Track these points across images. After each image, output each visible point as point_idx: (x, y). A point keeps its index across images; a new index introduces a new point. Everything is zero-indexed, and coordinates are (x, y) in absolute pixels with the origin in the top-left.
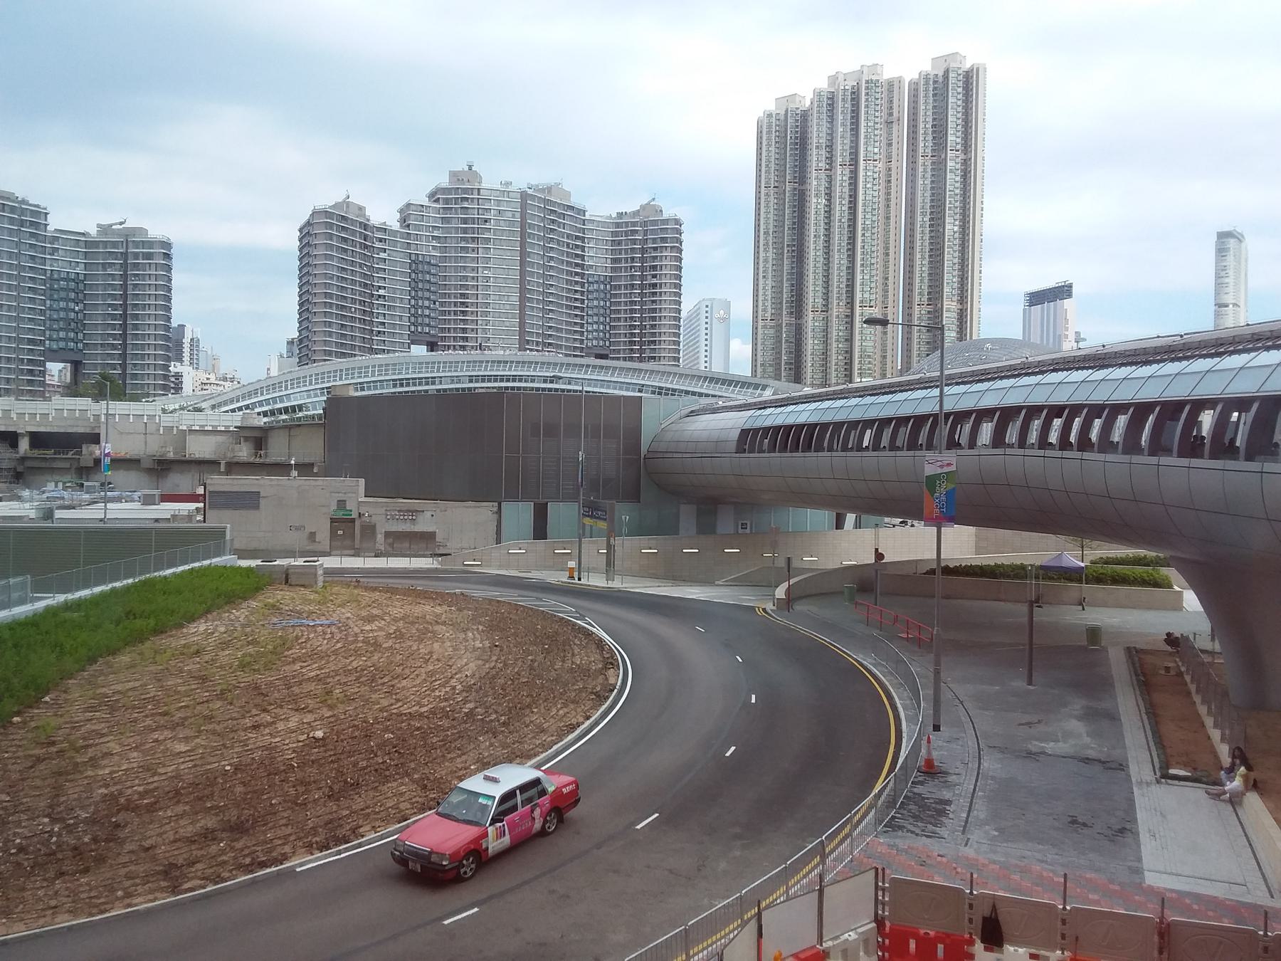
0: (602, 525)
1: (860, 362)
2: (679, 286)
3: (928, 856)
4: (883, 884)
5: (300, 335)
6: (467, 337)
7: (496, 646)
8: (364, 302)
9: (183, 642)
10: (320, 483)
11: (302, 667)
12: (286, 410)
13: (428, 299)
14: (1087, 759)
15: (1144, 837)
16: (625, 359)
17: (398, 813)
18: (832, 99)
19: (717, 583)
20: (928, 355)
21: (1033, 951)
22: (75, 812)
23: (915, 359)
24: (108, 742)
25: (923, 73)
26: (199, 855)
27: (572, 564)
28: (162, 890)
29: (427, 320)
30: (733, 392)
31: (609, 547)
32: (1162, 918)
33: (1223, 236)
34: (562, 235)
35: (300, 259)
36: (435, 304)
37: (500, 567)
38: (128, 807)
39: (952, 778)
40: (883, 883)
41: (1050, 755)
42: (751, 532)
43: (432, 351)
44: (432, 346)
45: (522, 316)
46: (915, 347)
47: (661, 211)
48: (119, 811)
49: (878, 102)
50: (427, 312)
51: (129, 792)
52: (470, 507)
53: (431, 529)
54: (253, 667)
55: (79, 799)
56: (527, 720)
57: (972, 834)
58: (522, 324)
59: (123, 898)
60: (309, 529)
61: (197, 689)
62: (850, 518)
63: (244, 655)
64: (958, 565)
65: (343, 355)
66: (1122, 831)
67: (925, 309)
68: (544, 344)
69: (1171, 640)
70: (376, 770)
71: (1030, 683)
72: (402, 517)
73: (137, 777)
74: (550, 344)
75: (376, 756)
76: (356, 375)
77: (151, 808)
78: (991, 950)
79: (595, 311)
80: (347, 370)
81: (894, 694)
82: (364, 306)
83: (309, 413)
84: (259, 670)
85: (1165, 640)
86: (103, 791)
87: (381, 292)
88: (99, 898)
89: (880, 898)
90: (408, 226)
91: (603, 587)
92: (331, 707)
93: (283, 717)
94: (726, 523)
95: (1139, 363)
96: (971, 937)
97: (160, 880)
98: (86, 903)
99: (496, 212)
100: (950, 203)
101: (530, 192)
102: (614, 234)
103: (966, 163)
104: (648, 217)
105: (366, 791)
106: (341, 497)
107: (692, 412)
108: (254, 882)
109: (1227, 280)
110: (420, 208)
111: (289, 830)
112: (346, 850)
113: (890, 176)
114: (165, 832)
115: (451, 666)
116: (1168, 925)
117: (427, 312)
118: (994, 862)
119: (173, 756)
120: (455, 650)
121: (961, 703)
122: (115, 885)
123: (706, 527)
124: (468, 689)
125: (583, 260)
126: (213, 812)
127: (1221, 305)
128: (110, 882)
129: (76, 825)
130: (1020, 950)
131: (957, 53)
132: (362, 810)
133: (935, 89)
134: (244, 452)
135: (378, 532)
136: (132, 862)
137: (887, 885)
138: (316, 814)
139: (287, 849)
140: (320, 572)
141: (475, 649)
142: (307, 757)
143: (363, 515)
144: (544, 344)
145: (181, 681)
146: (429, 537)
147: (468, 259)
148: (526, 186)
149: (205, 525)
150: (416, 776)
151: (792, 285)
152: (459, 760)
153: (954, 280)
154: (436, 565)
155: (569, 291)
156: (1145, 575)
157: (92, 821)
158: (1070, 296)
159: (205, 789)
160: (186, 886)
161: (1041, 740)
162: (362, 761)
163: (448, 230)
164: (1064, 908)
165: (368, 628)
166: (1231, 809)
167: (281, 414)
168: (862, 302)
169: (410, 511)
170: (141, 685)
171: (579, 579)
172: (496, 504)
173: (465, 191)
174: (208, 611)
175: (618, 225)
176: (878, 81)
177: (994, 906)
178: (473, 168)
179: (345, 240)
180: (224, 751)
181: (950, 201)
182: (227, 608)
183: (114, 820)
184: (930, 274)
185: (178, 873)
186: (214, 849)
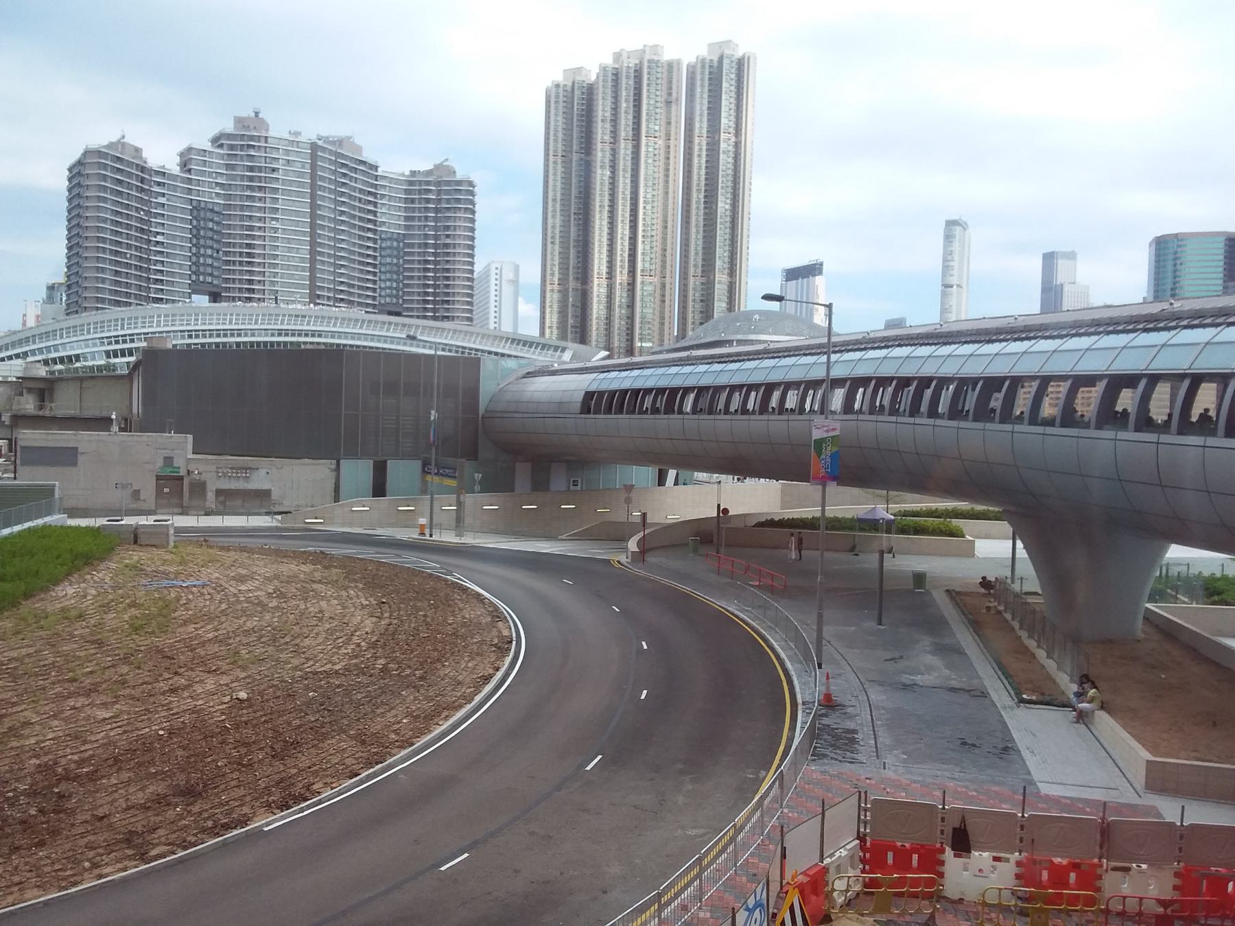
0: (453, 483)
1: (641, 328)
2: (472, 247)
3: (858, 780)
4: (866, 804)
5: (69, 280)
6: (254, 289)
7: (384, 603)
8: (141, 248)
9: (59, 606)
10: (144, 439)
11: (197, 629)
12: (62, 360)
13: (211, 247)
14: (954, 688)
15: (1026, 754)
16: (418, 317)
17: (346, 768)
18: (616, 75)
19: (560, 537)
20: (701, 324)
21: (995, 854)
22: (11, 784)
23: (690, 326)
24: (22, 711)
25: (700, 58)
26: (157, 822)
27: (423, 521)
28: (129, 857)
29: (209, 270)
30: (534, 353)
31: (459, 504)
32: (1103, 819)
33: (951, 224)
34: (354, 189)
35: (70, 201)
36: (218, 253)
37: (343, 525)
39: (849, 710)
40: (866, 804)
41: (922, 686)
42: (582, 489)
43: (215, 301)
44: (215, 297)
45: (312, 270)
46: (690, 316)
47: (455, 172)
48: (59, 781)
49: (659, 82)
50: (209, 261)
51: (63, 761)
52: (307, 464)
53: (265, 487)
54: (146, 630)
55: (11, 771)
56: (441, 673)
57: (886, 758)
58: (312, 278)
59: (91, 869)
60: (135, 487)
61: (97, 653)
62: (672, 474)
63: (131, 618)
64: (769, 518)
65: (118, 303)
66: (1006, 749)
67: (699, 280)
68: (336, 300)
69: (985, 583)
70: (311, 728)
71: (880, 624)
72: (234, 475)
73: (67, 746)
74: (342, 300)
75: (307, 714)
76: (140, 325)
77: (93, 777)
78: (960, 856)
79: (388, 268)
80: (130, 319)
81: (768, 637)
82: (141, 252)
83: (86, 364)
84: (153, 632)
85: (980, 583)
86: (34, 761)
87: (159, 238)
88: (65, 870)
89: (862, 817)
90: (189, 171)
91: (457, 543)
92: (244, 668)
93: (198, 679)
94: (559, 482)
95: (983, 341)
96: (942, 846)
97: (124, 848)
98: (52, 876)
99: (284, 162)
100: (723, 182)
101: (320, 143)
102: (407, 192)
103: (737, 145)
104: (441, 177)
105: (307, 749)
106: (168, 453)
107: (528, 373)
108: (224, 844)
109: (952, 264)
110: (202, 153)
111: (242, 792)
112: (309, 807)
113: (669, 152)
114: (116, 800)
115: (347, 624)
116: (1108, 824)
117: (209, 261)
118: (915, 782)
119: (98, 722)
120: (344, 608)
121: (829, 642)
122: (78, 856)
123: (540, 484)
124: (373, 645)
125: (375, 216)
126: (160, 778)
127: (947, 286)
128: (71, 853)
129: (16, 798)
130: (984, 854)
131: (731, 41)
132: (310, 768)
133: (710, 73)
134: (29, 405)
135: (208, 490)
136: (88, 832)
137: (869, 806)
138: (267, 773)
139: (246, 810)
140: (172, 532)
141: (363, 607)
142: (238, 719)
143: (192, 472)
144: (336, 300)
145: (75, 646)
146: (264, 495)
147: (254, 209)
148: (315, 137)
149: (16, 482)
150: (352, 733)
151: (579, 252)
152: (389, 715)
153: (725, 254)
154: (275, 524)
155: (361, 246)
156: (941, 526)
157: (32, 793)
158: (821, 273)
160: (153, 853)
161: (910, 674)
163: (233, 177)
164: (1023, 816)
165: (243, 588)
166: (1085, 727)
167: (56, 363)
168: (642, 271)
169: (244, 469)
170: (36, 652)
171: (431, 536)
172: (334, 462)
173: (252, 138)
174: (69, 574)
175: (411, 183)
176: (658, 61)
177: (963, 817)
178: (260, 116)
179: (120, 182)
180: (150, 715)
181: (723, 181)
182: (87, 570)
183: (57, 790)
184: (704, 248)
185: (140, 841)
186: (171, 814)
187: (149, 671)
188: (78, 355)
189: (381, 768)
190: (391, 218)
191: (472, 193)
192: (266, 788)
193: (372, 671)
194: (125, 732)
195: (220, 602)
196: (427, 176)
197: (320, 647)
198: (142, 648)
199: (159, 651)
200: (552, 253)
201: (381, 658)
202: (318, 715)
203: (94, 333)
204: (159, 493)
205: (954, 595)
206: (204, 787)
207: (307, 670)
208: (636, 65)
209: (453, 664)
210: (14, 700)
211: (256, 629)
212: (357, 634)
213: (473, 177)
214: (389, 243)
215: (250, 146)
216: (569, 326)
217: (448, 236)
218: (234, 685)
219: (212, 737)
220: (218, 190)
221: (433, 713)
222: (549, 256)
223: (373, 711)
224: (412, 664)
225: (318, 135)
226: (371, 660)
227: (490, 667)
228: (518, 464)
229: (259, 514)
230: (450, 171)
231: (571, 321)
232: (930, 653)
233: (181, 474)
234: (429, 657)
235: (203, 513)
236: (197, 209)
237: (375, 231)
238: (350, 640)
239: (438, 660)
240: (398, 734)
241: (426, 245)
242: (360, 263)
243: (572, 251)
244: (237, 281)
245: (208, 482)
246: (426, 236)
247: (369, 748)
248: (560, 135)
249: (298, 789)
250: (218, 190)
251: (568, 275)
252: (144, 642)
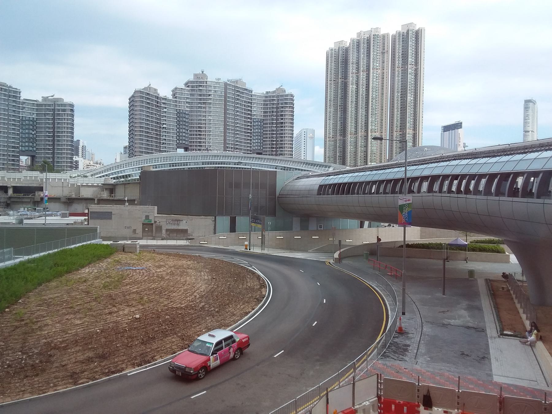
1: (371, 156)
2: (292, 123)
3: (400, 369)
4: (381, 381)
5: (129, 144)
6: (201, 145)
7: (214, 278)
8: (157, 130)
9: (79, 277)
10: (138, 208)
11: (130, 288)
12: (123, 177)
13: (185, 129)
14: (469, 327)
15: (493, 361)
16: (269, 155)
17: (172, 350)
18: (358, 42)
19: (309, 251)
20: (400, 153)
21: (445, 410)
22: (33, 350)
23: (394, 155)
24: (47, 320)
25: (398, 32)
26: (86, 368)
27: (246, 243)
28: (70, 383)
29: (184, 138)
30: (316, 169)
31: (263, 236)
32: (501, 395)
33: (527, 102)
34: (242, 101)
35: (129, 112)
36: (187, 131)
37: (215, 244)
39: (410, 335)
40: (381, 381)
41: (453, 325)
42: (324, 229)
43: (186, 151)
44: (186, 149)
45: (225, 136)
46: (394, 149)
47: (285, 91)
48: (51, 349)
49: (378, 44)
50: (184, 134)
51: (56, 341)
52: (203, 218)
53: (186, 228)
54: (109, 287)
55: (34, 344)
56: (227, 310)
57: (419, 359)
58: (225, 140)
59: (53, 387)
60: (133, 228)
62: (366, 223)
63: (105, 282)
64: (413, 243)
65: (148, 153)
66: (484, 358)
67: (399, 133)
68: (235, 148)
70: (162, 332)
71: (444, 294)
72: (173, 223)
73: (59, 335)
74: (237, 148)
75: (162, 326)
76: (153, 162)
77: (65, 348)
78: (427, 409)
79: (257, 134)
80: (150, 159)
81: (385, 299)
82: (157, 132)
83: (133, 178)
84: (111, 289)
85: (502, 276)
86: (45, 341)
87: (164, 126)
88: (43, 387)
89: (379, 387)
90: (176, 97)
91: (260, 253)
92: (143, 305)
93: (122, 309)
94: (313, 225)
95: (491, 156)
96: (418, 404)
97: (69, 379)
98: (37, 389)
99: (214, 91)
100: (409, 87)
101: (228, 83)
102: (265, 101)
103: (416, 70)
104: (279, 94)
105: (158, 341)
106: (147, 214)
107: (298, 177)
108: (109, 380)
109: (529, 121)
110: (181, 90)
111: (124, 358)
112: (149, 366)
113: (384, 76)
114: (71, 359)
115: (194, 287)
116: (503, 398)
117: (184, 134)
118: (429, 371)
119: (75, 326)
120: (196, 280)
121: (414, 303)
123: (304, 227)
124: (202, 297)
125: (251, 112)
126: (92, 350)
127: (526, 132)
128: (47, 380)
129: (33, 355)
130: (439, 409)
131: (412, 23)
132: (156, 349)
133: (403, 38)
134: (105, 195)
135: (163, 229)
136: (57, 371)
137: (382, 381)
138: (136, 351)
139: (124, 366)
140: (138, 246)
141: (205, 280)
142: (132, 326)
143: (157, 222)
144: (235, 148)
145: (78, 293)
146: (185, 231)
147: (201, 112)
148: (227, 80)
149: (88, 226)
150: (179, 334)
151: (341, 123)
152: (198, 327)
153: (411, 121)
155: (245, 125)
156: (493, 248)
157: (39, 354)
158: (461, 127)
160: (80, 382)
161: (449, 319)
162: (156, 328)
163: (193, 99)
164: (459, 391)
165: (159, 270)
166: (531, 348)
167: (121, 178)
168: (371, 130)
169: (177, 220)
170: (61, 295)
171: (250, 250)
172: (214, 217)
173: (201, 82)
174: (90, 263)
175: (266, 97)
176: (378, 35)
177: (428, 390)
178: (204, 73)
179: (148, 103)
180: (97, 323)
181: (409, 87)
182: (98, 262)
183: (49, 353)
184: (401, 118)
185: (77, 376)
186: (92, 366)
202: (167, 326)
205: (490, 283)
208: (368, 38)
232: (465, 310)
236: (180, 114)
239: (228, 304)
245: (163, 227)
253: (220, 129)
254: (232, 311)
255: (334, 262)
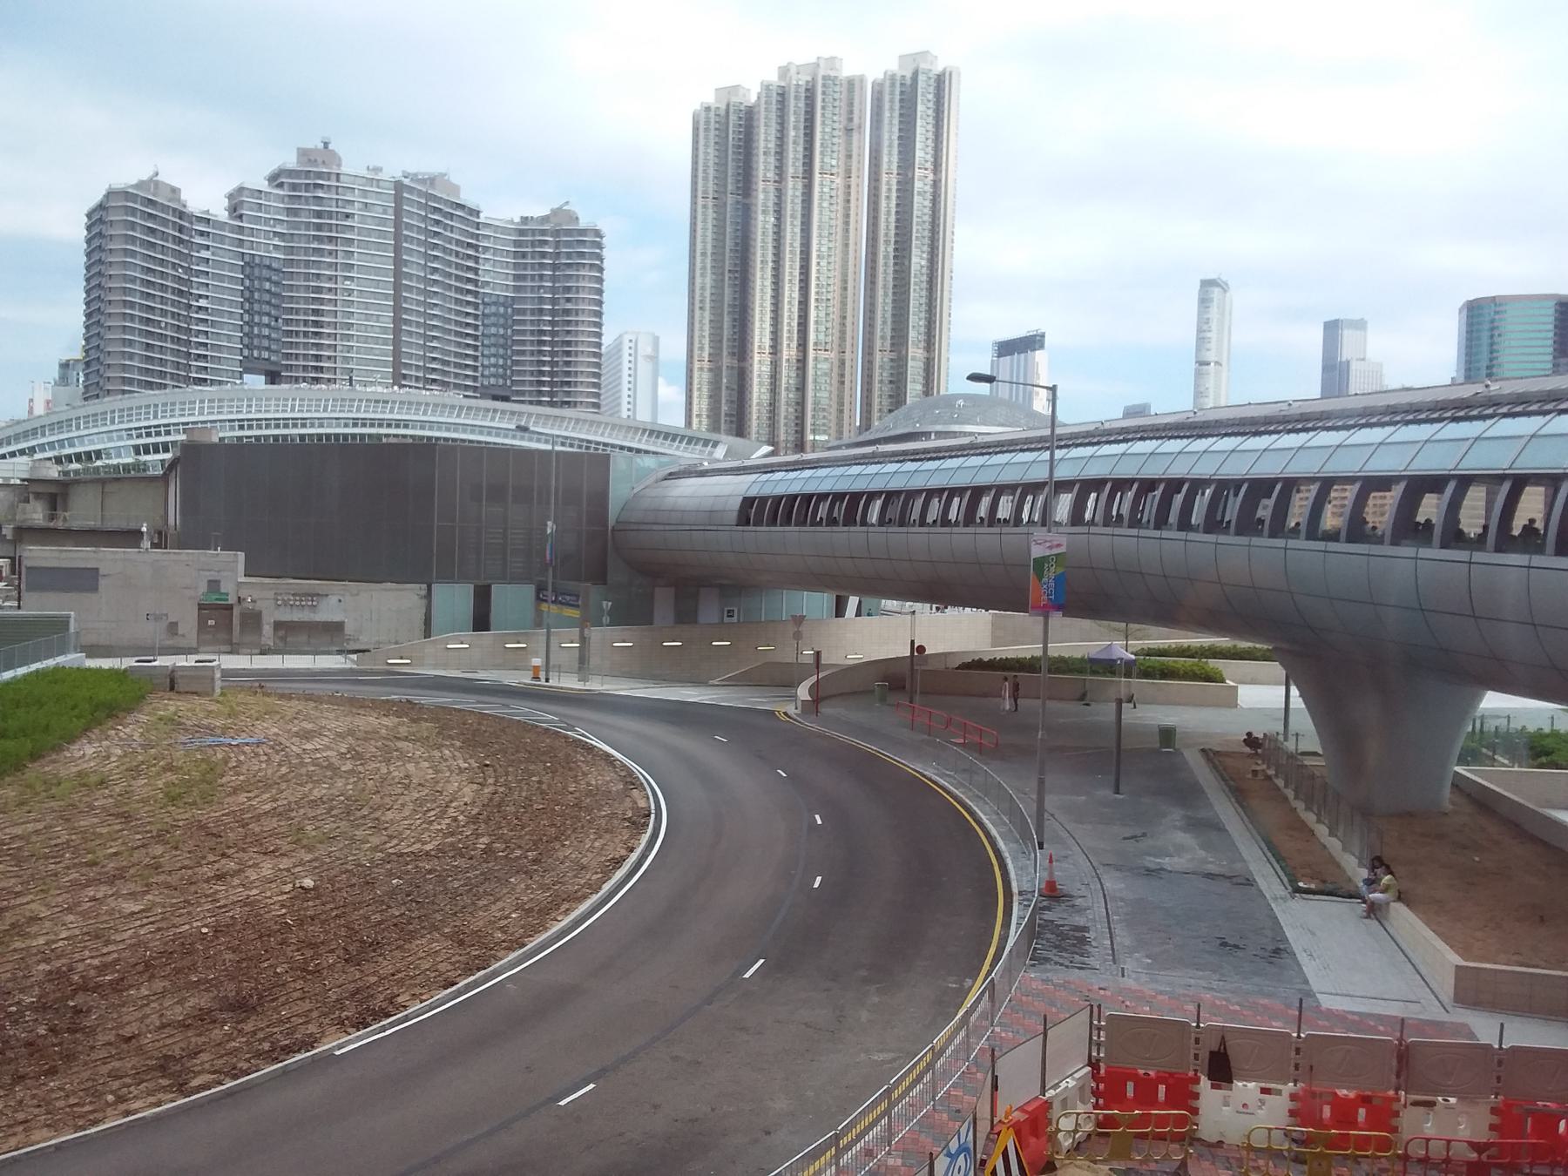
0: (575, 613)
1: (814, 416)
2: (599, 314)
3: (1089, 990)
4: (1099, 1022)
5: (87, 356)
6: (322, 367)
7: (487, 765)
8: (179, 314)
9: (74, 770)
10: (183, 557)
11: (249, 799)
12: (78, 457)
13: (268, 314)
14: (1211, 874)
15: (1302, 958)
16: (531, 403)
17: (439, 976)
18: (783, 95)
19: (711, 682)
20: (890, 411)
21: (1263, 1085)
22: (14, 996)
23: (876, 414)
24: (28, 903)
25: (889, 73)
26: (200, 1043)
27: (537, 661)
28: (164, 1089)
29: (266, 343)
30: (678, 448)
31: (583, 640)
32: (1401, 1040)
33: (1207, 284)
34: (450, 240)
35: (89, 255)
36: (276, 321)
37: (435, 666)
38: (84, 988)
39: (1078, 902)
40: (1099, 1022)
41: (1171, 872)
42: (739, 620)
43: (273, 383)
44: (273, 377)
45: (397, 342)
46: (876, 401)
47: (577, 218)
48: (75, 991)
49: (837, 104)
50: (266, 332)
51: (81, 967)
52: (390, 590)
53: (337, 618)
54: (186, 800)
55: (14, 979)
56: (560, 855)
57: (1125, 963)
58: (397, 353)
59: (115, 1103)
60: (172, 619)
62: (853, 602)
63: (167, 785)
64: (977, 658)
65: (150, 385)
66: (1277, 951)
67: (888, 356)
68: (427, 381)
69: (1251, 741)
70: (395, 925)
71: (1117, 792)
72: (298, 603)
73: (85, 947)
74: (434, 381)
75: (390, 907)
76: (177, 412)
77: (118, 987)
78: (1219, 1087)
79: (493, 340)
80: (165, 405)
81: (975, 808)
82: (179, 321)
83: (110, 462)
84: (194, 803)
85: (1245, 740)
86: (43, 967)
87: (202, 303)
88: (83, 1105)
89: (1095, 1038)
90: (241, 217)
91: (580, 690)
92: (310, 849)
93: (251, 863)
94: (709, 612)
95: (1247, 433)
96: (1196, 1074)
97: (158, 1077)
98: (66, 1113)
99: (361, 206)
100: (917, 231)
101: (406, 181)
102: (517, 243)
103: (936, 184)
104: (560, 225)
105: (390, 951)
106: (213, 575)
107: (670, 474)
108: (285, 1072)
109: (1209, 335)
110: (256, 194)
111: (307, 1005)
112: (392, 1025)
113: (849, 194)
114: (147, 1016)
115: (441, 792)
116: (1407, 1047)
117: (266, 332)
118: (1161, 993)
119: (125, 917)
120: (437, 772)
121: (1052, 815)
123: (685, 615)
124: (474, 820)
125: (477, 274)
126: (203, 987)
127: (1203, 363)
128: (90, 1084)
129: (21, 1013)
130: (1249, 1084)
131: (928, 52)
132: (393, 975)
133: (902, 93)
134: (36, 514)
135: (264, 622)
136: (112, 1056)
137: (1103, 1023)
138: (339, 981)
139: (312, 1028)
140: (218, 675)
141: (461, 771)
142: (302, 912)
143: (244, 599)
144: (427, 381)
145: (96, 820)
146: (336, 628)
147: (322, 265)
148: (400, 174)
149: (20, 612)
150: (446, 930)
151: (735, 320)
152: (494, 908)
153: (921, 323)
155: (458, 313)
156: (1195, 668)
157: (41, 1007)
158: (1042, 347)
159: (182, 959)
160: (195, 1083)
161: (1155, 856)
162: (373, 914)
163: (296, 225)
164: (1299, 1037)
165: (309, 746)
166: (1377, 923)
167: (71, 462)
168: (816, 344)
169: (309, 595)
170: (45, 828)
171: (547, 680)
172: (424, 586)
173: (320, 175)
174: (87, 729)
175: (522, 232)
176: (836, 77)
177: (1223, 1038)
178: (331, 147)
179: (152, 231)
180: (191, 908)
181: (917, 230)
182: (110, 724)
183: (72, 1004)
184: (893, 315)
185: (178, 1068)
186: (217, 1034)
187: (189, 852)
188: (100, 450)
189: (484, 975)
190: (496, 277)
191: (599, 246)
192: (337, 1000)
193: (472, 853)
194: (159, 929)
195: (280, 765)
196: (542, 224)
197: (406, 822)
198: (181, 823)
199: (202, 827)
200: (701, 321)
201: (483, 835)
203: (120, 422)
204: (202, 626)
205: (1212, 756)
206: (259, 999)
207: (390, 851)
208: (807, 82)
209: (576, 843)
210: (18, 889)
211: (325, 799)
212: (453, 805)
213: (601, 225)
214: (493, 309)
215: (317, 186)
216: (723, 414)
217: (568, 300)
218: (297, 870)
219: (269, 936)
220: (276, 242)
221: (549, 906)
222: (697, 325)
223: (474, 904)
224: (523, 843)
225: (403, 172)
226: (471, 838)
227: (622, 848)
228: (657, 590)
229: (329, 653)
230: (571, 217)
231: (724, 408)
233: (230, 602)
234: (545, 835)
235: (258, 651)
237: (476, 294)
238: (445, 812)
240: (505, 932)
241: (541, 311)
242: (457, 334)
243: (726, 318)
244: (301, 357)
246: (541, 300)
247: (468, 950)
248: (711, 172)
249: (378, 1002)
250: (276, 242)
251: (721, 349)
252: (182, 815)
253: (381, 319)
254: (574, 856)
255: (796, 711)
